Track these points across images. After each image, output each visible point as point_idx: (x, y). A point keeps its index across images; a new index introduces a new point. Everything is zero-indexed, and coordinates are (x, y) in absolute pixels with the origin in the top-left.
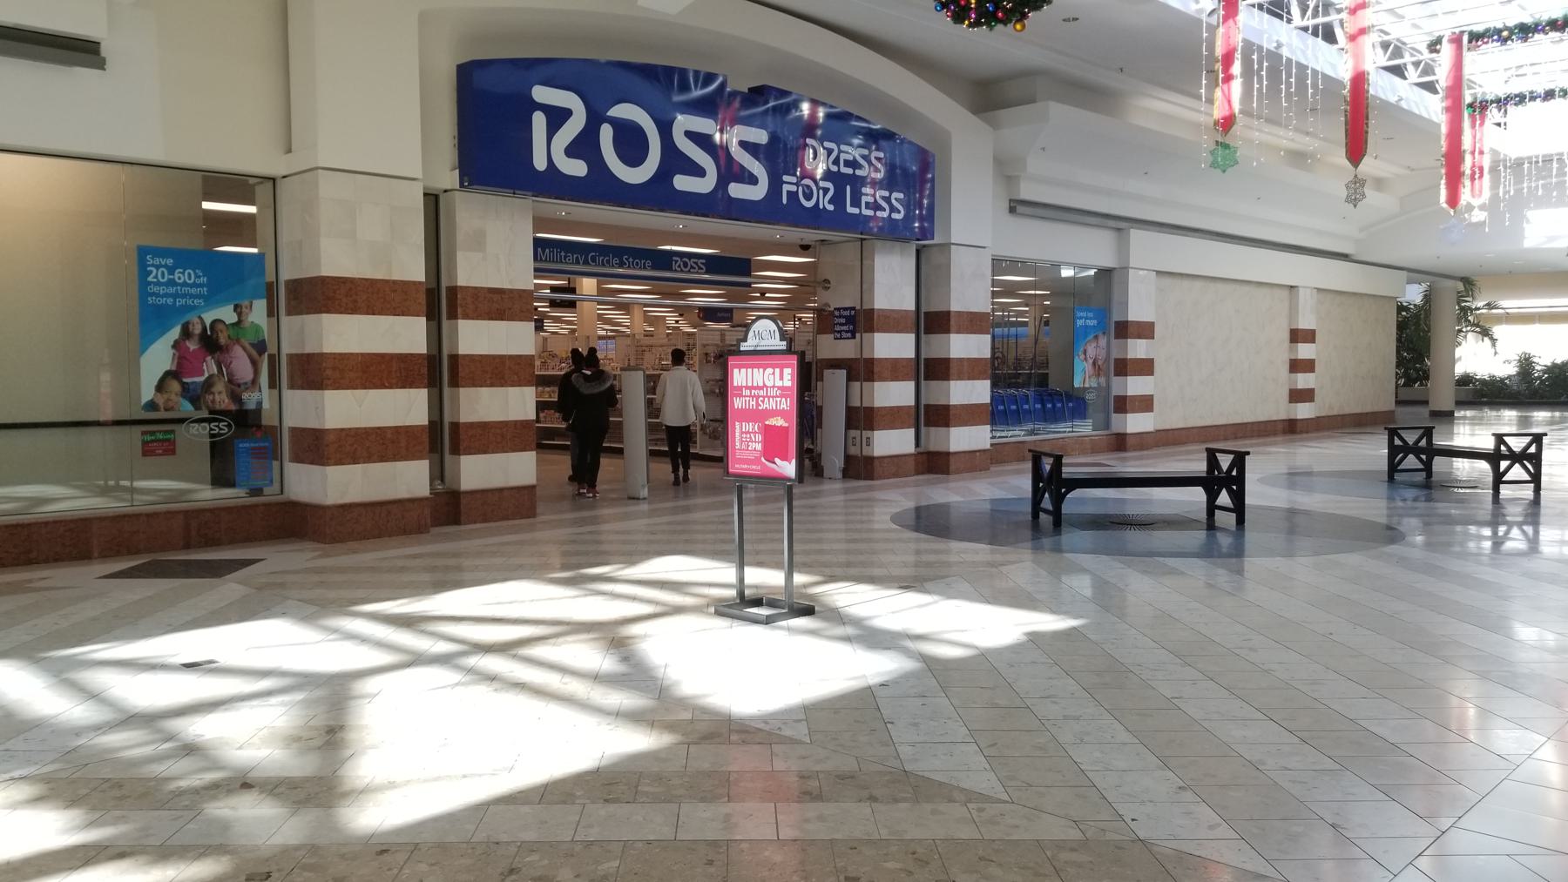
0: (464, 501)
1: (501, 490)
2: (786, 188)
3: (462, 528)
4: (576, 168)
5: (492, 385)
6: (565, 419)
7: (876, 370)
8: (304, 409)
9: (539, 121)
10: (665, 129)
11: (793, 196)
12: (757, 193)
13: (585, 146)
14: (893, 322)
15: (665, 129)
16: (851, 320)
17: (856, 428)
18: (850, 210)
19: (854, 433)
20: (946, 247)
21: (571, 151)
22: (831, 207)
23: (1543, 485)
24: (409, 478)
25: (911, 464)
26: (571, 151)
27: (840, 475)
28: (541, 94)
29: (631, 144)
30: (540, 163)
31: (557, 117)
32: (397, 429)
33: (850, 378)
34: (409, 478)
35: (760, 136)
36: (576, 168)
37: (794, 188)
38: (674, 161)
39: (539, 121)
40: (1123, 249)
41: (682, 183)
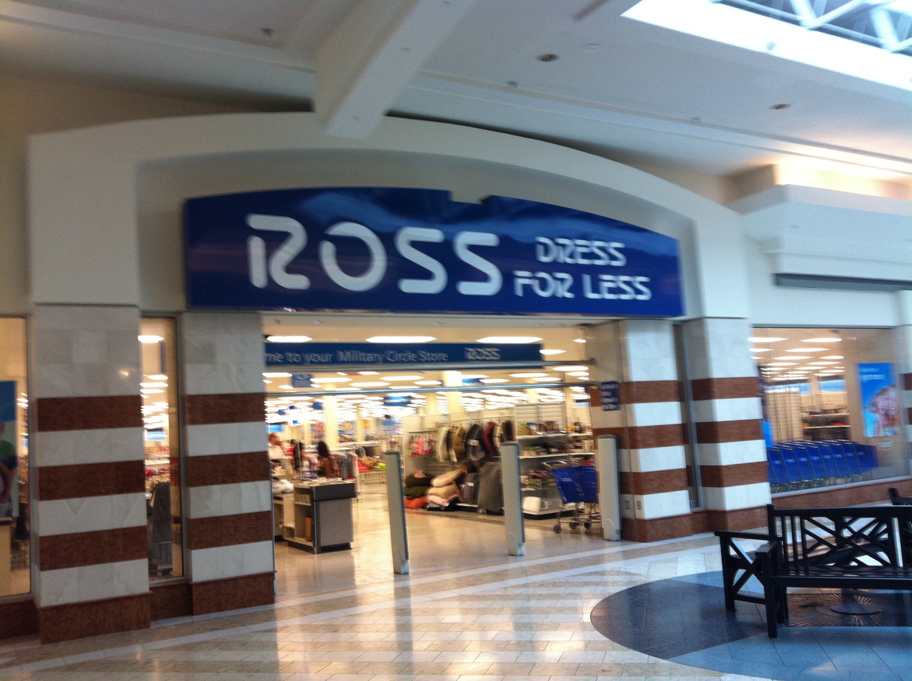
0: (195, 592)
1: (235, 580)
2: (520, 282)
3: (196, 618)
4: (299, 282)
5: (224, 482)
6: (319, 458)
7: (639, 437)
8: (788, 522)
9: (256, 246)
10: (388, 240)
11: (527, 288)
12: (490, 288)
13: (306, 262)
14: (652, 392)
15: (388, 240)
16: (614, 393)
17: (629, 493)
18: (591, 296)
19: (628, 497)
20: (700, 321)
21: (291, 268)
22: (569, 295)
23: (811, 507)
24: (131, 577)
25: (688, 523)
26: (291, 268)
27: (617, 537)
28: (257, 221)
29: (353, 255)
30: (258, 279)
31: (275, 240)
32: (114, 533)
33: (620, 445)
34: (131, 577)
35: (488, 239)
36: (299, 282)
37: (527, 282)
38: (401, 268)
39: (256, 246)
40: (900, 309)
41: (409, 286)
